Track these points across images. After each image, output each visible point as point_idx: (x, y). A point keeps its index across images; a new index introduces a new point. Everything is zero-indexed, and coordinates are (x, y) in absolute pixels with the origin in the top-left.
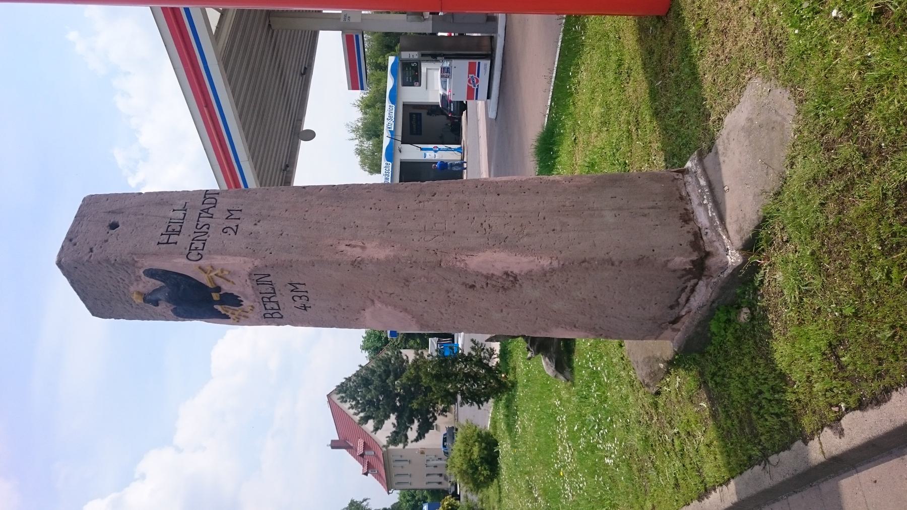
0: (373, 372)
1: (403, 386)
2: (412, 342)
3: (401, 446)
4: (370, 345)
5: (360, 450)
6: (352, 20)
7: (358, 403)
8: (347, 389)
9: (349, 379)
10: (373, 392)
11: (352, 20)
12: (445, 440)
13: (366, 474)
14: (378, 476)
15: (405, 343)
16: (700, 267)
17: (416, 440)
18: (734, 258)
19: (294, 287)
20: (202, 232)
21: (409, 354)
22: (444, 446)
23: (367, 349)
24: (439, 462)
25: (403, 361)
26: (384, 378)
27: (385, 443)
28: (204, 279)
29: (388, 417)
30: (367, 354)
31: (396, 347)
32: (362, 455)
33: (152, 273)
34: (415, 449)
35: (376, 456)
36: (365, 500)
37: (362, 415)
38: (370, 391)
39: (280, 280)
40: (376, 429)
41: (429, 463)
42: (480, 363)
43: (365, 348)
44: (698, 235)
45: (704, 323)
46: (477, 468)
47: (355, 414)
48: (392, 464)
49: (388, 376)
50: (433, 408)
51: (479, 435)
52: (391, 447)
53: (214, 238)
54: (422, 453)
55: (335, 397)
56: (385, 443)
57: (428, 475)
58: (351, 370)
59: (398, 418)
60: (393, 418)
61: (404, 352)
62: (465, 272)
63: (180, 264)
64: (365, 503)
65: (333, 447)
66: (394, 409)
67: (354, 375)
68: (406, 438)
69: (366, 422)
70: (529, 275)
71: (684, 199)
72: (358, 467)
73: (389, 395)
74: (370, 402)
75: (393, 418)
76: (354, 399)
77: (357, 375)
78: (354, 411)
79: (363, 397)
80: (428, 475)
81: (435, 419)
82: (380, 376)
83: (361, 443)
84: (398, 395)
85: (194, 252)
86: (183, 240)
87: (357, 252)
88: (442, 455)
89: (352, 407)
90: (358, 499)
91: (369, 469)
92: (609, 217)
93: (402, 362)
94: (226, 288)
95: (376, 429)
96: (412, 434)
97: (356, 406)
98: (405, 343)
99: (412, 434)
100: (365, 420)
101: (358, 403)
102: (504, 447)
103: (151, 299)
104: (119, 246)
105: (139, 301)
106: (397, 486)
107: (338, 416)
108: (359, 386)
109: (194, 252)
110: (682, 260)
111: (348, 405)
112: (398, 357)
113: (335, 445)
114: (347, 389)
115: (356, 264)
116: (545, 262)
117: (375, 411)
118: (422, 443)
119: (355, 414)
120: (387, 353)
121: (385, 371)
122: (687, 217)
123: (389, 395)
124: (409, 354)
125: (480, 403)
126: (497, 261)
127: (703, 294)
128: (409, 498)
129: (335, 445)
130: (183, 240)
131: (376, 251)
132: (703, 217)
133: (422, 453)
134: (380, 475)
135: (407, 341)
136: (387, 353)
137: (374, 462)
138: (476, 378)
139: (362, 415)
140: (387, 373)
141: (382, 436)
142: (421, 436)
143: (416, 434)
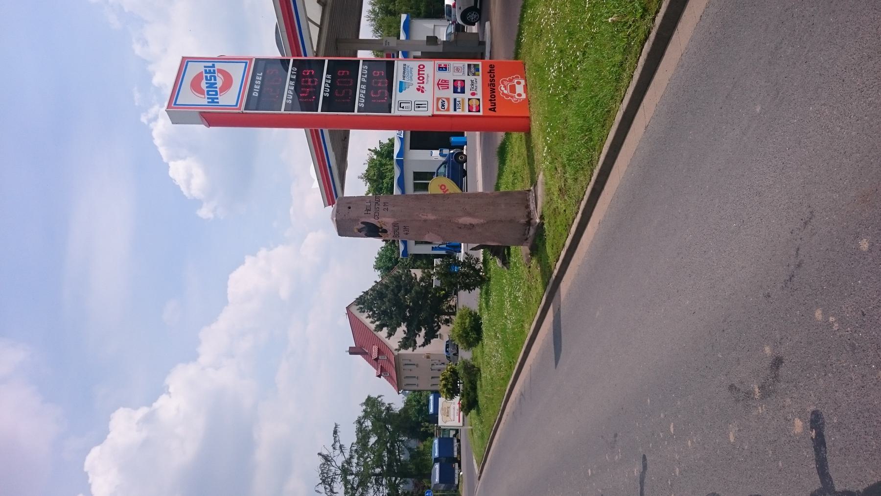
0: (387, 287)
1: (412, 301)
2: (419, 263)
3: (411, 349)
4: (382, 265)
5: (375, 355)
6: (391, 45)
7: (374, 313)
8: (365, 301)
9: (366, 293)
10: (387, 303)
11: (391, 45)
12: (447, 346)
13: (379, 376)
14: (390, 379)
15: (414, 263)
16: (529, 223)
17: (423, 345)
18: (538, 221)
19: (405, 227)
20: (377, 210)
21: (418, 273)
22: (447, 351)
23: (379, 269)
24: (443, 366)
25: (412, 278)
26: (396, 292)
27: (397, 347)
28: (378, 225)
29: (400, 325)
30: (379, 273)
31: (407, 267)
32: (377, 360)
33: (363, 223)
34: (421, 355)
35: (389, 360)
36: (379, 397)
37: (378, 323)
38: (384, 303)
39: (401, 225)
40: (390, 335)
41: (433, 367)
42: (470, 266)
43: (377, 267)
44: (529, 213)
45: (534, 240)
46: (468, 333)
47: (372, 322)
48: (402, 365)
49: (399, 291)
50: (438, 317)
51: (470, 313)
52: (403, 351)
53: (381, 212)
54: (428, 357)
55: (355, 310)
56: (397, 347)
57: (433, 378)
58: (368, 285)
59: (407, 326)
60: (403, 327)
61: (413, 271)
62: (458, 224)
63: (372, 220)
64: (379, 399)
65: (351, 353)
66: (405, 319)
67: (371, 289)
68: (415, 343)
69: (381, 329)
70: (478, 225)
71: (528, 201)
72: (373, 372)
73: (400, 306)
74: (384, 312)
75: (403, 327)
76: (371, 310)
77: (373, 289)
78: (371, 319)
79: (379, 308)
80: (433, 378)
81: (440, 328)
82: (392, 290)
83: (375, 349)
84: (408, 306)
85: (376, 216)
86: (372, 212)
87: (425, 217)
88: (445, 360)
89: (369, 317)
90: (374, 395)
91: (382, 372)
92: (503, 206)
93: (411, 278)
94: (384, 227)
95: (390, 335)
96: (420, 340)
97: (373, 316)
98: (414, 263)
99: (420, 340)
100: (380, 328)
101: (374, 313)
102: (485, 318)
103: (360, 231)
104: (353, 214)
105: (356, 231)
106: (406, 388)
107: (356, 326)
108: (375, 299)
109: (376, 216)
110: (523, 221)
111: (366, 314)
112: (408, 275)
113: (352, 351)
114: (365, 301)
115: (425, 221)
116: (482, 221)
117: (388, 321)
118: (428, 349)
119: (372, 322)
120: (397, 271)
121: (397, 286)
122: (528, 207)
123: (400, 306)
124: (418, 273)
125: (470, 290)
126: (467, 220)
127: (532, 231)
128: (414, 403)
129: (352, 351)
130: (372, 212)
131: (431, 217)
132: (532, 207)
133: (428, 357)
134: (392, 378)
135: (415, 261)
136: (397, 271)
137: (386, 365)
138: (467, 275)
139: (378, 323)
140: (399, 288)
141: (394, 343)
142: (427, 342)
143: (423, 340)
